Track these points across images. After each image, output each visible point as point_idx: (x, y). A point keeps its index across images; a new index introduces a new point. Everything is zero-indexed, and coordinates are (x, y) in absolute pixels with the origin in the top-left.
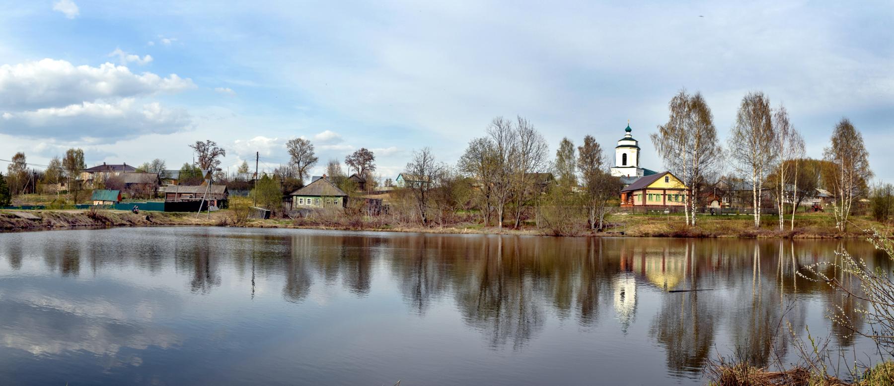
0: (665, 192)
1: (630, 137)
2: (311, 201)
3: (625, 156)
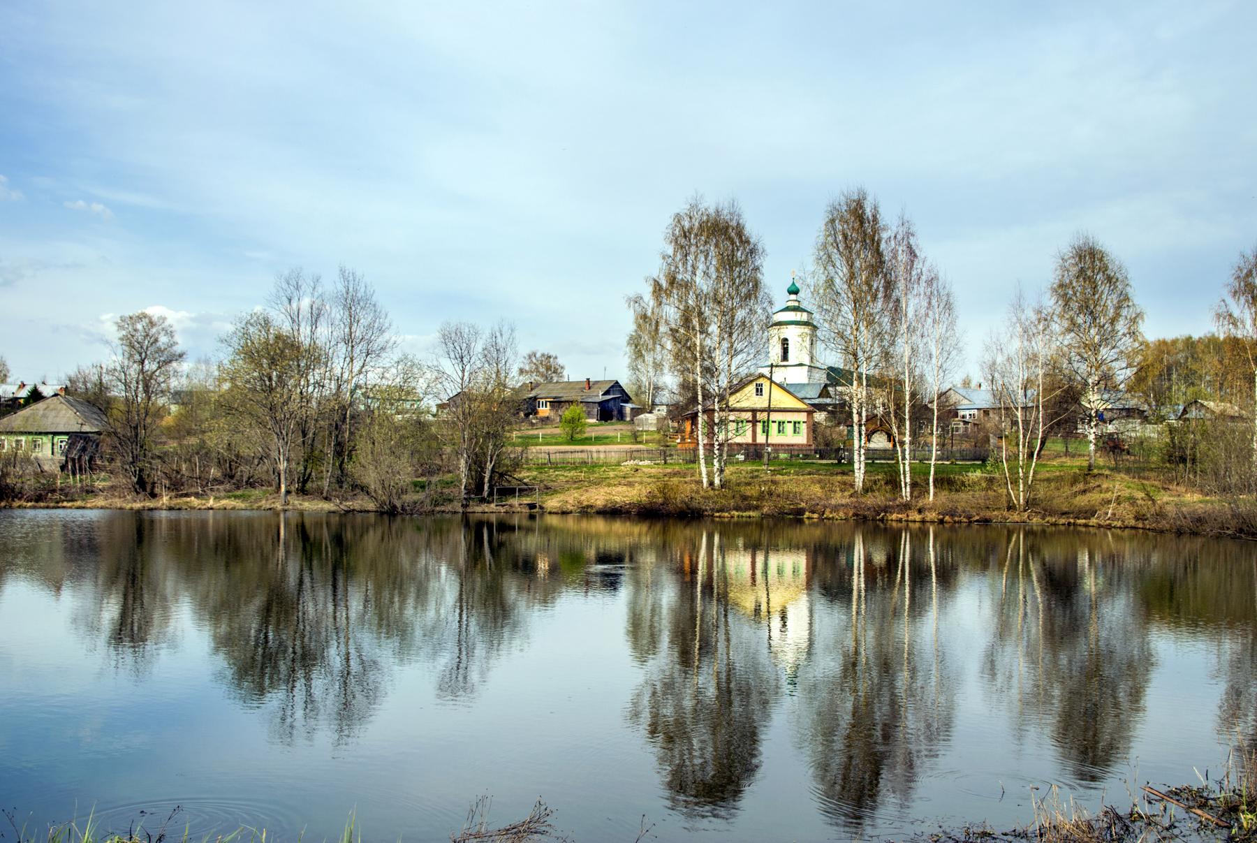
0: (754, 416)
1: (796, 304)
2: (23, 444)
3: (785, 342)
